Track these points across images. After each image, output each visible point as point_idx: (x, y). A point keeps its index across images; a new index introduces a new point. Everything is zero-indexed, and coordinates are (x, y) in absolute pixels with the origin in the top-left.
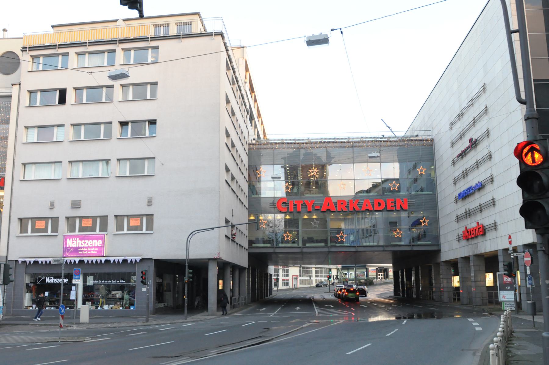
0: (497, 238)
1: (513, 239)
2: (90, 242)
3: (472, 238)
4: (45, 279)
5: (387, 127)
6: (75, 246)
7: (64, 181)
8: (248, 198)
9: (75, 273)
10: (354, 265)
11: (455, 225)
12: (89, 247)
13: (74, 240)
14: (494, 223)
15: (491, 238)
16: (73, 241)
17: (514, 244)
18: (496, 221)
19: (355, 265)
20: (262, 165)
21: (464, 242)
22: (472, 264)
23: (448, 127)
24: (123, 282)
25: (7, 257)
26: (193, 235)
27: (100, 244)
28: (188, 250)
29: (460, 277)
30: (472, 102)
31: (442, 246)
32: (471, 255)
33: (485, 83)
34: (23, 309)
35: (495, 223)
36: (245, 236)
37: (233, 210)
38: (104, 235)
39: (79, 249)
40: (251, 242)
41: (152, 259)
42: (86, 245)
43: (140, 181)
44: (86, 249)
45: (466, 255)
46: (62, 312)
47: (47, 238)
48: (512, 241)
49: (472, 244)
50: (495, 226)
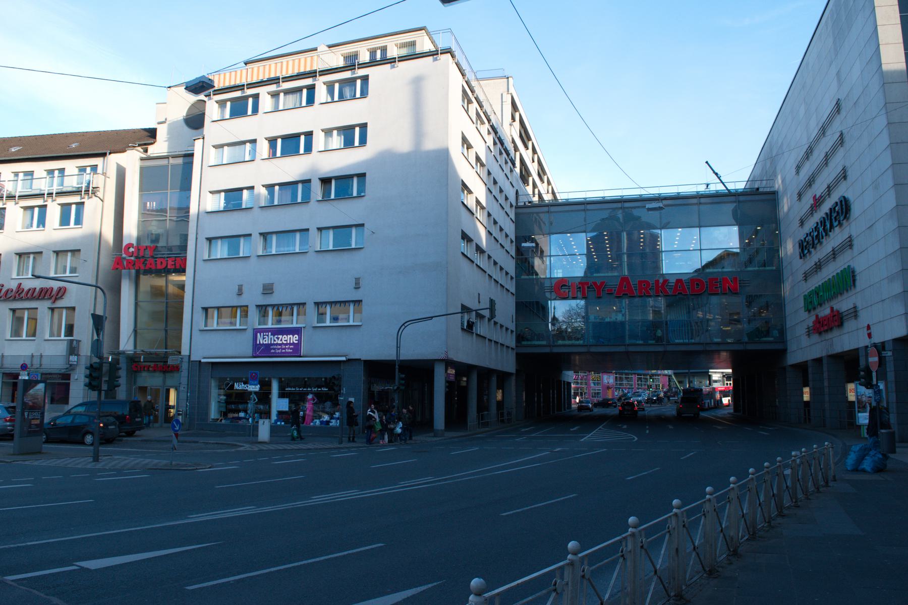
0: (857, 329)
1: (873, 330)
2: (285, 338)
3: (826, 331)
4: (233, 385)
5: (714, 174)
6: (267, 342)
7: (254, 260)
8: (516, 280)
9: (251, 376)
10: (687, 371)
11: (803, 315)
12: (283, 344)
13: (266, 335)
14: (853, 308)
15: (850, 331)
16: (265, 337)
17: (877, 339)
18: (857, 305)
19: (689, 370)
20: (537, 235)
21: (815, 338)
22: (825, 368)
23: (794, 171)
24: (325, 389)
25: (189, 356)
26: (406, 327)
27: (296, 340)
28: (398, 347)
29: (810, 389)
30: (823, 131)
31: (789, 343)
32: (825, 356)
33: (839, 99)
34: (209, 422)
35: (855, 307)
36: (509, 332)
37: (479, 294)
38: (301, 328)
39: (272, 347)
40: (520, 338)
41: (360, 359)
42: (280, 342)
43: (346, 256)
44: (280, 347)
45: (818, 356)
46: (176, 429)
47: (235, 332)
48: (872, 333)
49: (825, 340)
50: (856, 311)
